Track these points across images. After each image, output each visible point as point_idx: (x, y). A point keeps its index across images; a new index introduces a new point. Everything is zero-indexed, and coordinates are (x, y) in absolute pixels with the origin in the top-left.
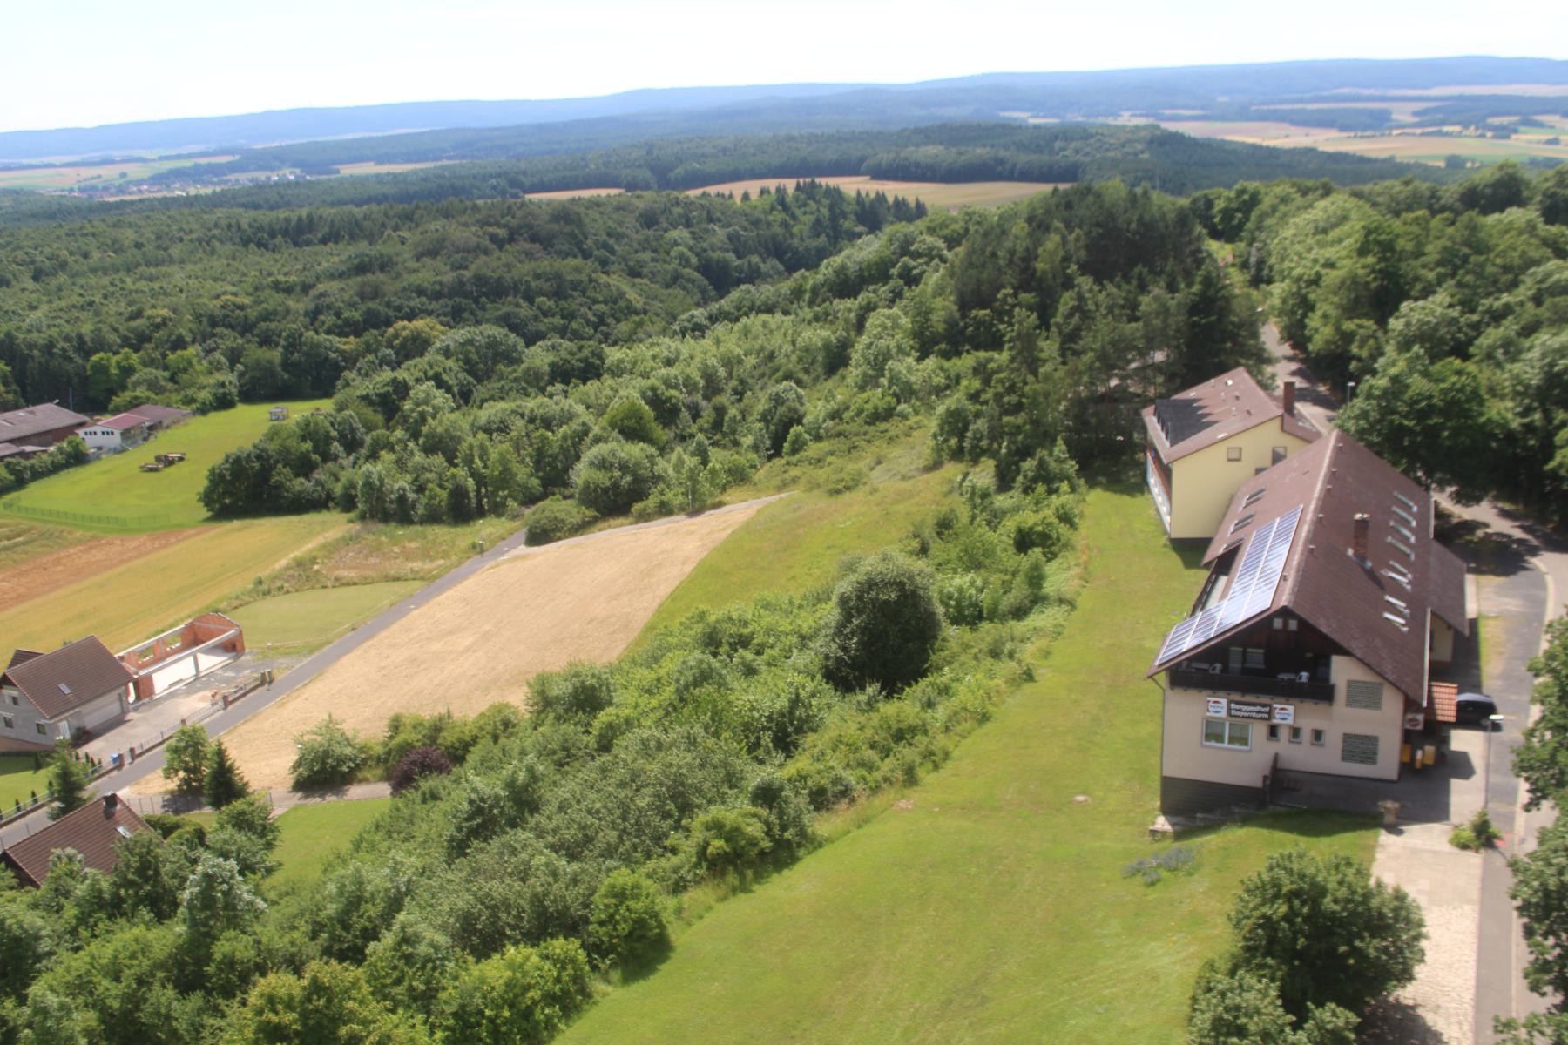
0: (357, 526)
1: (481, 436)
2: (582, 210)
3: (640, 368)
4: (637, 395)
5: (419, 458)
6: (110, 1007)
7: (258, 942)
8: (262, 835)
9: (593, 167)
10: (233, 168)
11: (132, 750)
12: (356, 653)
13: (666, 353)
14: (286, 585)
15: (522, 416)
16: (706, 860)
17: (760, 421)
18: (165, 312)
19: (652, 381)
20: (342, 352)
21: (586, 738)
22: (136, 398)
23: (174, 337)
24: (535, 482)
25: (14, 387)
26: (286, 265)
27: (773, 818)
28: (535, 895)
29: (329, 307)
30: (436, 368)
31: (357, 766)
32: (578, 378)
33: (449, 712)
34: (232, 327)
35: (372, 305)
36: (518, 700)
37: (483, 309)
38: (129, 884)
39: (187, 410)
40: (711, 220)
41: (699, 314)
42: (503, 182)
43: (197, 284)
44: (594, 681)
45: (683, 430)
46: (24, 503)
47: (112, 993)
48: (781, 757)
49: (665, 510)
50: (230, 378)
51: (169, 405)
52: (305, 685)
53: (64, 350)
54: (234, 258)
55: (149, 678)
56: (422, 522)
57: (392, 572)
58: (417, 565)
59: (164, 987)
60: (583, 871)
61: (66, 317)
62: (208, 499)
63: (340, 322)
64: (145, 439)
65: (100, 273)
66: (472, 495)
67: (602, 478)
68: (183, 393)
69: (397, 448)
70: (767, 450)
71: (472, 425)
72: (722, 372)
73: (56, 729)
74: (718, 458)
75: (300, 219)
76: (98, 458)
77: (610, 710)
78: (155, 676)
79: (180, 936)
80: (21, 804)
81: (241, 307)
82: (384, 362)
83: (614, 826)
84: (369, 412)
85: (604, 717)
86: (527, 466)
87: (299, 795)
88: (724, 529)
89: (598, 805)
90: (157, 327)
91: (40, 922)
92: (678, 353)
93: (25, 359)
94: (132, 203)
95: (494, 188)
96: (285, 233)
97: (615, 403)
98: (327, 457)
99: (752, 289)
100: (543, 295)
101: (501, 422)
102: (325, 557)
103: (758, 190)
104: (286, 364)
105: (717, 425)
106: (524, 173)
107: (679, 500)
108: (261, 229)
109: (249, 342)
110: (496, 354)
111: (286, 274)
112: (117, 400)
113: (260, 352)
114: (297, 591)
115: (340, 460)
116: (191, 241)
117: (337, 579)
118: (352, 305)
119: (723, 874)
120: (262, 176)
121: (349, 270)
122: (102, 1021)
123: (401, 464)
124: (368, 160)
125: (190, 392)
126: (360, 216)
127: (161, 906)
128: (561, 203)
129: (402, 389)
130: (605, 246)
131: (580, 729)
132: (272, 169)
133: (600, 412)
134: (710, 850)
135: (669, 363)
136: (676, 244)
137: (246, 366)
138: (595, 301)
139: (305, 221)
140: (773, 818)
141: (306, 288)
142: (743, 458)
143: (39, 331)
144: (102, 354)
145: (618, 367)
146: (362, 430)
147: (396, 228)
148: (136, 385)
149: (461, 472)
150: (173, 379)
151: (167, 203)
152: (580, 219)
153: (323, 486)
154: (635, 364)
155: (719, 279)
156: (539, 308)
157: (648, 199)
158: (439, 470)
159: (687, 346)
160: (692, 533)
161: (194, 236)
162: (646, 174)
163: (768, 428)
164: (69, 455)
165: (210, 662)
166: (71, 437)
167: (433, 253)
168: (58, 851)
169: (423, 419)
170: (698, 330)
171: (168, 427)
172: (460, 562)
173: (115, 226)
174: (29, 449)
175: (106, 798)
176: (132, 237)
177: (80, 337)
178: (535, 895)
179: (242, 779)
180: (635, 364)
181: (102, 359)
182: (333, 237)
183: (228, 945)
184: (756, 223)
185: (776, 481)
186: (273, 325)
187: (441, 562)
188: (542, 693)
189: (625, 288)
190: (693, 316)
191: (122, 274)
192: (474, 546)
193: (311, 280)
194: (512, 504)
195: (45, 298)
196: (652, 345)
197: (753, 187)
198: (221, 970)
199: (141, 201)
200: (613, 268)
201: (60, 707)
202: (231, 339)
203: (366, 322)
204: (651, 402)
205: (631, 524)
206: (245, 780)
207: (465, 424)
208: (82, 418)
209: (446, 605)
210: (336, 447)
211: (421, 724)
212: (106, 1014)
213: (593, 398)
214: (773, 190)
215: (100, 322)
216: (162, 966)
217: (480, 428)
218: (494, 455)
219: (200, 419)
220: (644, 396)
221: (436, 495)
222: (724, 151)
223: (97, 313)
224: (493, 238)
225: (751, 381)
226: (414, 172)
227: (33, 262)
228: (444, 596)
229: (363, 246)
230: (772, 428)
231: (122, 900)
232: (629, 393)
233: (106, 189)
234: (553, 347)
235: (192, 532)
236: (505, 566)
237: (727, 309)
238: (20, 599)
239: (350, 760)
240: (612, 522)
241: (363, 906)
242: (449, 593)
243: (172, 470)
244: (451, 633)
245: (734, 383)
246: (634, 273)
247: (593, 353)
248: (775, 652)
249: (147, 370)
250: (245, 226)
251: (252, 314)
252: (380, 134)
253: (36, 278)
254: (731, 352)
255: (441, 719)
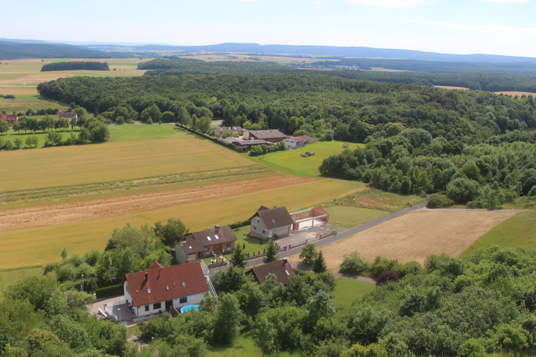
0: (369, 189)
1: (417, 166)
2: (457, 94)
3: (476, 153)
4: (475, 163)
5: (394, 169)
6: (282, 330)
7: (331, 323)
8: (330, 286)
9: (459, 79)
10: (338, 63)
11: (290, 246)
12: (365, 231)
13: (486, 150)
14: (344, 203)
15: (431, 162)
16: (502, 344)
17: (520, 181)
18: (315, 107)
19: (479, 159)
20: (369, 129)
21: (452, 284)
22: (302, 132)
23: (317, 115)
24: (432, 186)
25: (267, 123)
26: (355, 97)
27: (531, 336)
28: (440, 339)
29: (367, 114)
30: (402, 140)
31: (362, 270)
32: (452, 153)
33: (397, 260)
34: (335, 115)
35: (381, 115)
36: (422, 262)
37: (418, 123)
38: (290, 291)
39: (317, 139)
40: (502, 104)
41: (498, 137)
42: (427, 80)
43: (326, 100)
44: (458, 263)
45: (489, 178)
46: (265, 159)
47: (283, 326)
48: (528, 311)
49: (479, 206)
50: (332, 131)
51: (312, 137)
52: (346, 238)
53: (283, 114)
54: (338, 93)
55: (298, 224)
56: (390, 192)
57: (379, 207)
58: (388, 206)
59: (299, 329)
60: (457, 335)
61: (285, 103)
62: (321, 169)
63: (370, 119)
64: (303, 146)
65: (296, 91)
66: (410, 186)
67: (457, 190)
68: (317, 133)
69: (387, 165)
70: (521, 192)
71: (414, 162)
72: (506, 160)
73: (268, 233)
74: (502, 192)
75: (361, 83)
76: (288, 149)
77: (463, 276)
78: (300, 224)
79: (307, 314)
80: (255, 254)
81: (339, 109)
82: (382, 135)
83: (467, 321)
84: (377, 151)
85: (460, 278)
86: (431, 180)
87: (341, 275)
88: (503, 218)
89: (462, 312)
90: (312, 111)
91: (263, 295)
92: (491, 150)
93: (272, 115)
94: (306, 70)
95: (423, 82)
96: (355, 87)
97: (466, 165)
98: (362, 163)
99: (519, 132)
100: (439, 122)
101: (424, 163)
102: (357, 196)
103: (521, 95)
104: (350, 130)
105: (502, 179)
106: (434, 78)
107: (486, 203)
108: (347, 85)
109: (339, 121)
110: (422, 139)
111: (354, 100)
112: (296, 132)
113: (343, 124)
114: (347, 206)
115: (365, 165)
116: (325, 85)
117: (360, 205)
118: (375, 114)
119: (508, 351)
120: (347, 67)
121: (375, 102)
122: (278, 334)
123: (387, 171)
124: (381, 67)
125: (319, 133)
126: (381, 85)
127: (301, 301)
128: (450, 90)
129: (390, 146)
130: (463, 108)
131: (450, 280)
132: (350, 66)
133: (460, 166)
134: (504, 341)
135: (486, 153)
136: (489, 110)
137: (337, 128)
138: (457, 126)
139: (363, 84)
140: (531, 336)
141: (361, 106)
142: (512, 194)
143: (277, 107)
144: (295, 117)
145: (467, 151)
146: (374, 156)
147: (392, 91)
148: (303, 128)
149: (407, 177)
150: (314, 128)
151: (317, 72)
152: (456, 97)
153: (358, 173)
154: (474, 152)
155: (502, 126)
156: (437, 125)
157: (480, 93)
158: (400, 175)
159: (492, 148)
160: (489, 216)
161: (326, 84)
162: (478, 84)
163: (522, 184)
164: (280, 147)
165: (317, 223)
166: (281, 141)
167: (404, 101)
168: (270, 274)
169: (397, 157)
170: (496, 143)
171: (310, 144)
172: (403, 209)
173: (302, 77)
174: (269, 142)
175: (284, 260)
176: (307, 81)
177: (289, 111)
178: (440, 339)
179: (325, 265)
180: (474, 152)
181: (294, 118)
182: (370, 91)
183: (322, 322)
184: (519, 107)
185: (524, 204)
186: (348, 117)
187: (396, 207)
188: (431, 262)
189: (469, 123)
190: (495, 138)
191: (303, 93)
192: (408, 204)
193: (362, 104)
194: (423, 192)
195: (279, 97)
196: (481, 146)
197: (520, 94)
198: (318, 329)
199: (309, 70)
200: (465, 116)
201: (270, 226)
202: (334, 119)
203: (378, 120)
204: (478, 166)
205: (466, 208)
206: (326, 265)
207: (411, 161)
208: (284, 136)
209: (397, 222)
210: (365, 161)
211: (387, 262)
212: (280, 331)
213: (457, 160)
214: (527, 96)
215: (295, 107)
216: (298, 321)
217: (416, 164)
218: (420, 174)
219: (320, 143)
220: (476, 163)
221: (398, 184)
222: (508, 80)
223: (294, 104)
224: (425, 99)
225: (516, 165)
226: (396, 73)
227: (277, 85)
228: (397, 219)
229: (380, 95)
230: (524, 184)
231: (287, 296)
232: (472, 162)
233: (298, 65)
234: (442, 140)
235: (314, 179)
236: (419, 213)
237: (508, 137)
238: (260, 189)
239: (360, 267)
240: (459, 206)
241: (369, 322)
242: (398, 218)
243: (310, 158)
244: (398, 232)
245: (510, 165)
246: (472, 119)
247: (459, 145)
248: (526, 269)
249: (307, 124)
250: (343, 83)
251: (342, 112)
252: (386, 59)
253: (277, 90)
254: (510, 153)
255: (394, 262)
